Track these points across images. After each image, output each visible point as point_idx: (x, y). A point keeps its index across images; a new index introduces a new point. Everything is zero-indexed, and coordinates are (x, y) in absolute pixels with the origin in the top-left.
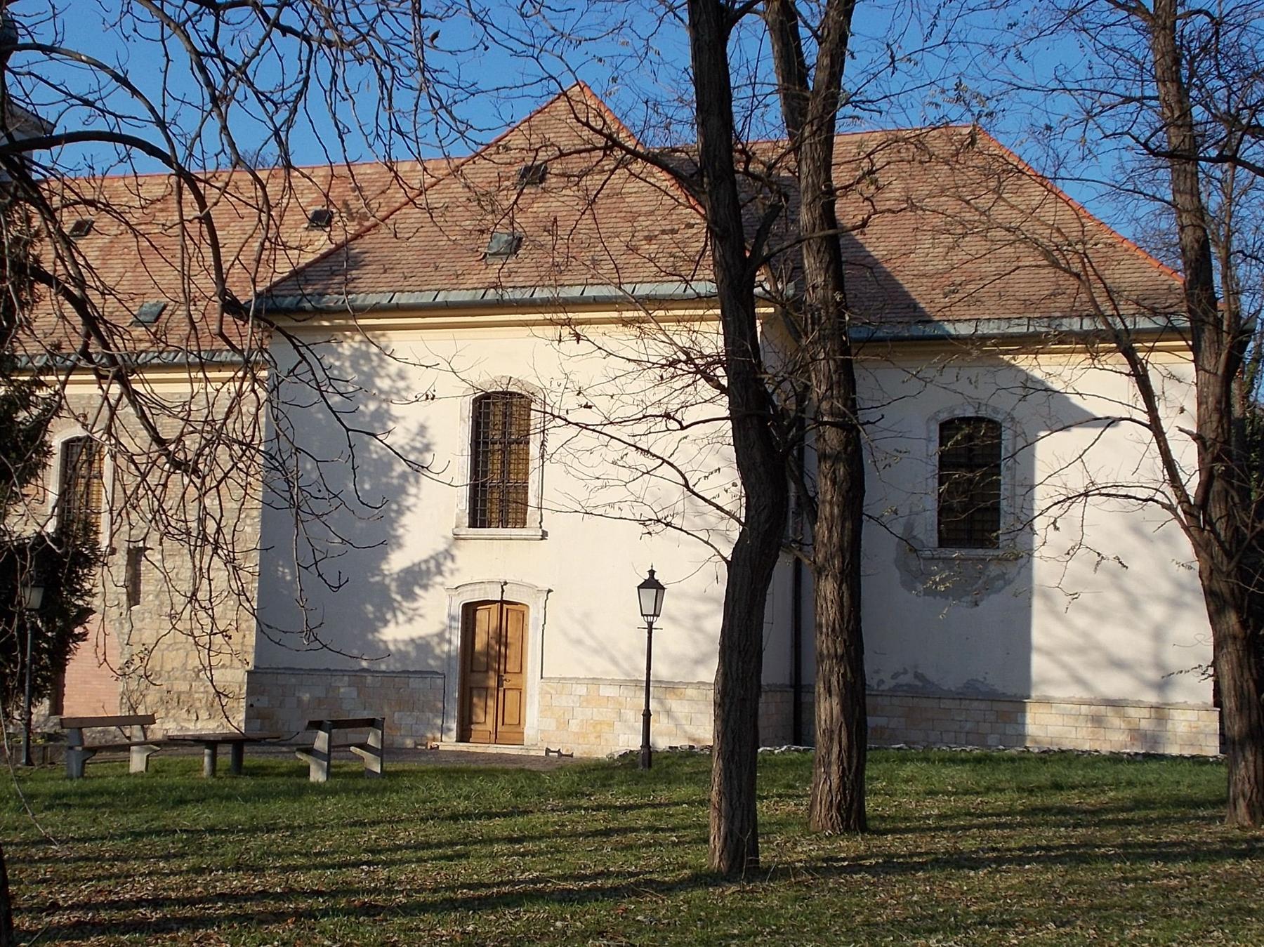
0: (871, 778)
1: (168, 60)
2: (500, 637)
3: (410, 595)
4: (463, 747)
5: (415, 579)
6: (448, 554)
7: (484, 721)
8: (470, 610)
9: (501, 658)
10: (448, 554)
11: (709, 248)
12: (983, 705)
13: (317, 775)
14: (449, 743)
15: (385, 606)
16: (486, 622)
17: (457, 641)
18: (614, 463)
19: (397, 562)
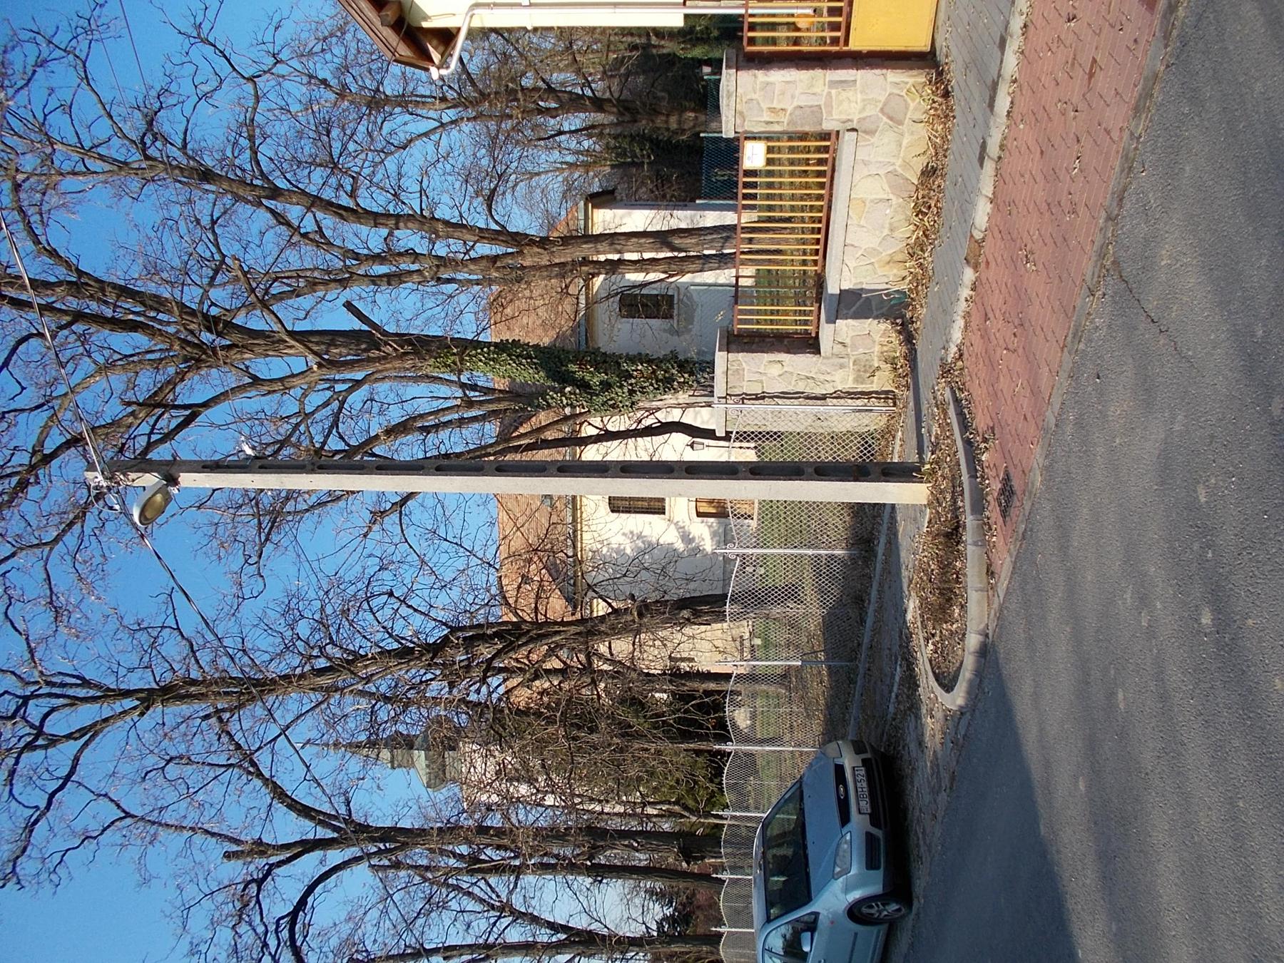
0: (250, 130)
1: (106, 795)
2: (711, 502)
3: (693, 540)
4: (755, 517)
5: (686, 538)
6: (676, 524)
7: (745, 509)
8: (699, 514)
9: (719, 502)
10: (676, 524)
11: (522, 430)
12: (420, 862)
13: (762, 571)
14: (754, 524)
15: (698, 550)
16: (704, 508)
17: (712, 520)
18: (1094, 60)
19: (680, 546)
